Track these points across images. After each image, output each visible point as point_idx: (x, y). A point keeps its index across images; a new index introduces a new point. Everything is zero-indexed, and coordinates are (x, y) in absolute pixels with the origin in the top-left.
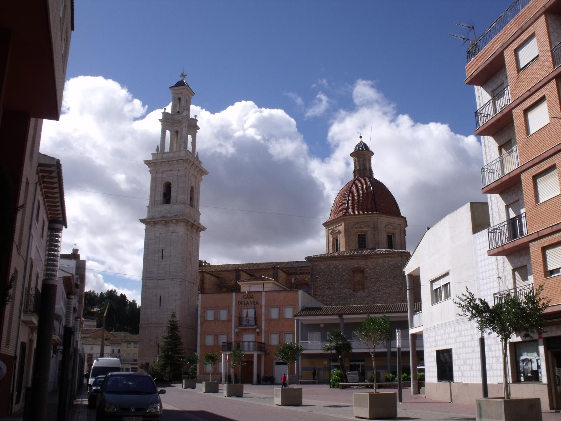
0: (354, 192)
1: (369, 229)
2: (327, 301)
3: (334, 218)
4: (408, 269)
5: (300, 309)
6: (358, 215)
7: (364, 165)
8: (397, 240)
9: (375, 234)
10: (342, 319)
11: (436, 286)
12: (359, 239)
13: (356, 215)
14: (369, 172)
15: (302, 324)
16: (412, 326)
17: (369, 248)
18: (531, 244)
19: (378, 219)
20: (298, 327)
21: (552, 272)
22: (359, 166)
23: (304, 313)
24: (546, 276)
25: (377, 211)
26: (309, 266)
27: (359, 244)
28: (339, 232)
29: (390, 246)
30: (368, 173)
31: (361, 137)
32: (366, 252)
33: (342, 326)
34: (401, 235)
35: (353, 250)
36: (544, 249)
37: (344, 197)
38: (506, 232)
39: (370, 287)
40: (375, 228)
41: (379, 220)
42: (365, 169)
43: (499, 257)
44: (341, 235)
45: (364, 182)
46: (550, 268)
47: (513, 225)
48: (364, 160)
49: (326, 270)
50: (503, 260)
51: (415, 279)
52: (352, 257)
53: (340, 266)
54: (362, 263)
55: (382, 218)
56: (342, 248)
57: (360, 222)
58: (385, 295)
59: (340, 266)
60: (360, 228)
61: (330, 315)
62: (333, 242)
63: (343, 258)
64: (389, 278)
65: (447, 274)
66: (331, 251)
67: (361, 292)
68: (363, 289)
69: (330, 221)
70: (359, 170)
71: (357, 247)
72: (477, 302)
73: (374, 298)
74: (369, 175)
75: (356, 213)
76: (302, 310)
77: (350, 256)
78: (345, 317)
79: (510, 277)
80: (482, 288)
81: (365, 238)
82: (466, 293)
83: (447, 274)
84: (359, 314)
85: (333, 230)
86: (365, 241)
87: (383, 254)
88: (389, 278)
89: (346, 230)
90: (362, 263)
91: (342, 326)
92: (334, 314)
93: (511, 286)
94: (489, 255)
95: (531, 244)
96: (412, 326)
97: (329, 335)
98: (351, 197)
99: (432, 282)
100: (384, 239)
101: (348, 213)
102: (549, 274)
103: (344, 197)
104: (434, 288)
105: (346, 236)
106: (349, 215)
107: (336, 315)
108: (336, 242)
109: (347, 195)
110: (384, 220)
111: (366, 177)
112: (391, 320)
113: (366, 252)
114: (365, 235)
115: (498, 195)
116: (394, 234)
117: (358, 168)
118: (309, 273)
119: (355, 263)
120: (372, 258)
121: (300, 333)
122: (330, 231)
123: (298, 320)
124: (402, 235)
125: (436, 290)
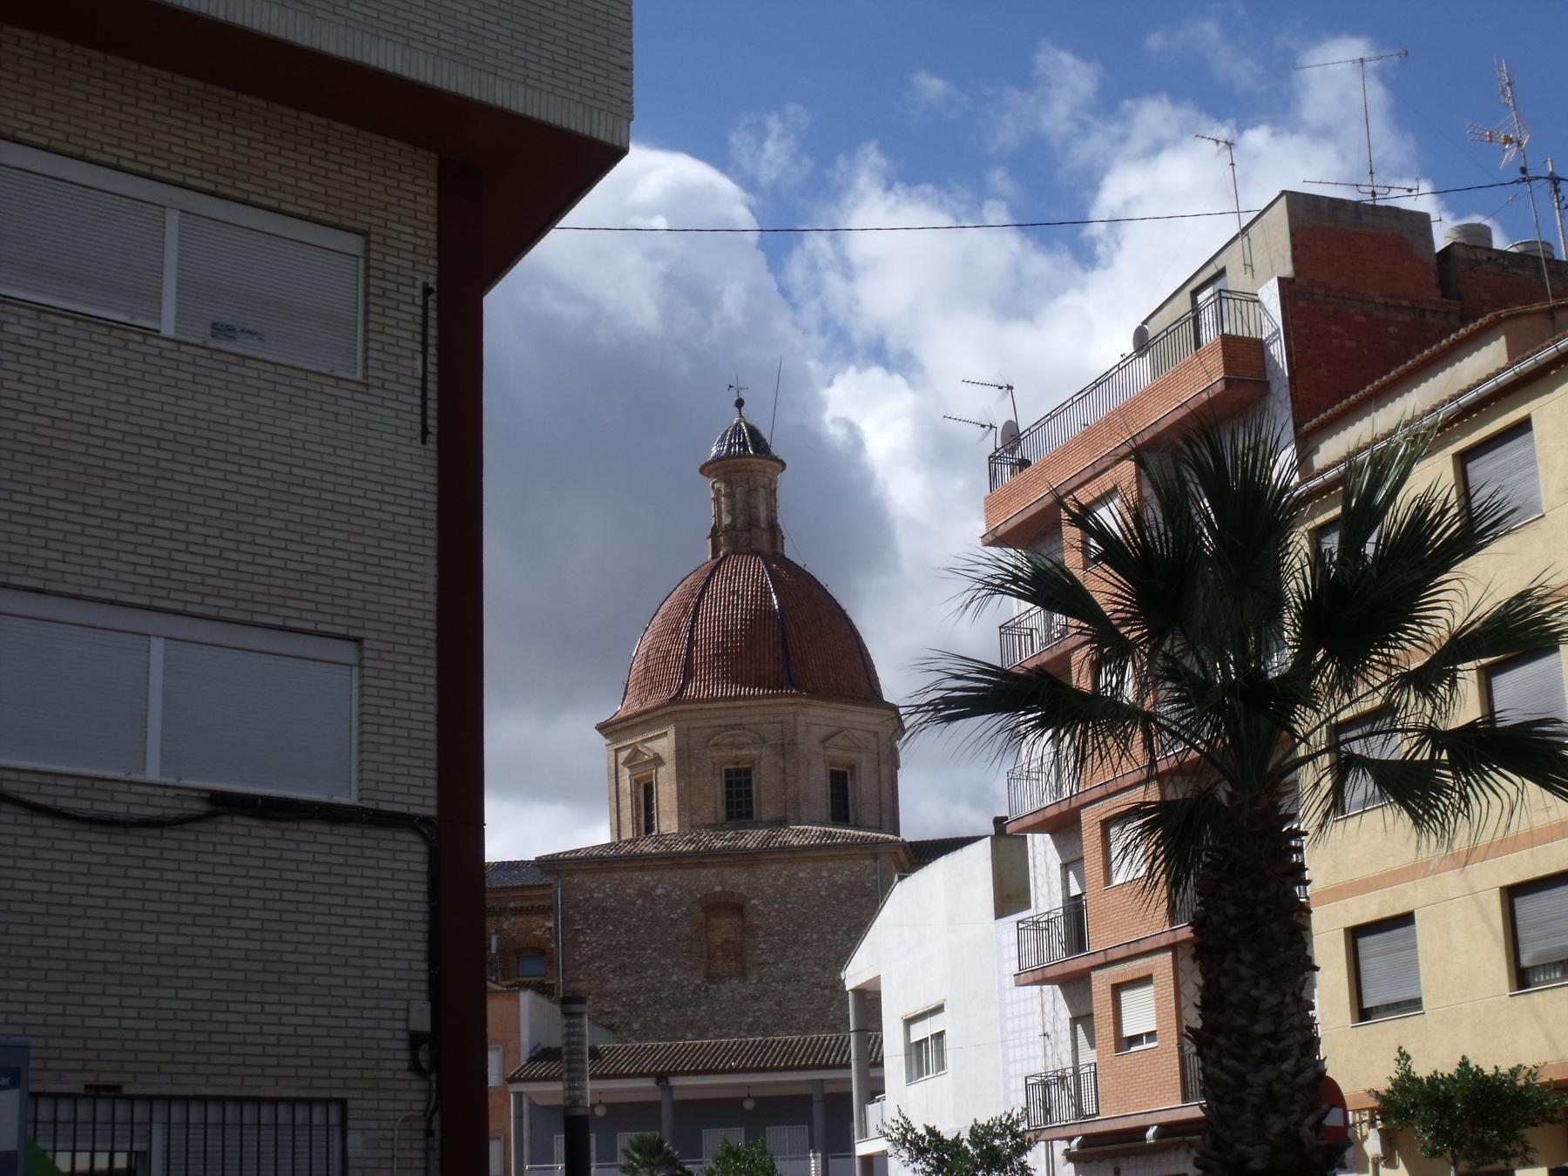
0: (712, 610)
1: (765, 751)
2: (613, 1014)
3: (636, 708)
4: (855, 975)
5: (525, 1054)
6: (724, 699)
7: (750, 508)
8: (863, 787)
9: (784, 770)
10: (669, 1089)
11: (920, 1031)
12: (728, 784)
13: (717, 700)
14: (766, 537)
15: (533, 1105)
16: (864, 1134)
17: (765, 817)
18: (1094, 974)
19: (796, 714)
20: (519, 1117)
21: (1136, 1039)
22: (732, 511)
23: (541, 1068)
24: (1118, 1048)
25: (794, 686)
26: (549, 886)
27: (729, 805)
28: (658, 761)
29: (840, 812)
30: (764, 543)
31: (740, 403)
32: (752, 839)
33: (666, 1113)
34: (878, 772)
35: (707, 826)
36: (1117, 989)
37: (676, 630)
38: (1062, 928)
39: (763, 964)
40: (785, 748)
41: (801, 719)
42: (752, 524)
43: (1046, 988)
44: (662, 770)
45: (749, 573)
46: (1128, 1031)
47: (1075, 910)
48: (751, 492)
49: (611, 903)
50: (1053, 993)
51: (869, 998)
52: (701, 859)
53: (659, 891)
54: (736, 879)
55: (811, 711)
56: (668, 822)
57: (732, 727)
58: (817, 991)
59: (659, 891)
60: (732, 746)
61: (628, 1076)
62: (634, 794)
63: (673, 860)
64: (834, 933)
65: (939, 1009)
66: (628, 834)
67: (735, 983)
68: (743, 974)
69: (625, 719)
70: (732, 527)
71: (722, 814)
72: (921, 1131)
73: (779, 1004)
74: (766, 548)
75: (717, 691)
76: (531, 1060)
77: (696, 853)
78: (676, 1081)
79: (1066, 1036)
80: (1011, 1056)
81: (749, 783)
82: (897, 1117)
83: (939, 1009)
84: (723, 1072)
85: (636, 753)
86: (749, 793)
87: (810, 847)
88: (834, 933)
89: (683, 755)
90: (736, 879)
91: (666, 1113)
92: (641, 1075)
93: (1067, 1061)
94: (1018, 985)
95: (1094, 974)
96: (864, 1134)
97: (626, 1152)
98: (699, 634)
99: (909, 1022)
100: (817, 785)
101: (690, 691)
102: (1125, 1044)
103: (676, 630)
104: (914, 1038)
105: (682, 775)
106: (693, 700)
107: (648, 1075)
108: (646, 796)
109: (686, 623)
110: (817, 719)
111: (758, 553)
112: (829, 1089)
113: (752, 839)
114: (748, 772)
115: (1047, 836)
116: (852, 768)
117: (726, 520)
118: (547, 911)
119: (712, 881)
120: (773, 861)
121: (526, 1135)
122: (623, 755)
123: (519, 1095)
124: (885, 771)
125: (919, 1043)
